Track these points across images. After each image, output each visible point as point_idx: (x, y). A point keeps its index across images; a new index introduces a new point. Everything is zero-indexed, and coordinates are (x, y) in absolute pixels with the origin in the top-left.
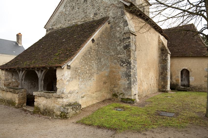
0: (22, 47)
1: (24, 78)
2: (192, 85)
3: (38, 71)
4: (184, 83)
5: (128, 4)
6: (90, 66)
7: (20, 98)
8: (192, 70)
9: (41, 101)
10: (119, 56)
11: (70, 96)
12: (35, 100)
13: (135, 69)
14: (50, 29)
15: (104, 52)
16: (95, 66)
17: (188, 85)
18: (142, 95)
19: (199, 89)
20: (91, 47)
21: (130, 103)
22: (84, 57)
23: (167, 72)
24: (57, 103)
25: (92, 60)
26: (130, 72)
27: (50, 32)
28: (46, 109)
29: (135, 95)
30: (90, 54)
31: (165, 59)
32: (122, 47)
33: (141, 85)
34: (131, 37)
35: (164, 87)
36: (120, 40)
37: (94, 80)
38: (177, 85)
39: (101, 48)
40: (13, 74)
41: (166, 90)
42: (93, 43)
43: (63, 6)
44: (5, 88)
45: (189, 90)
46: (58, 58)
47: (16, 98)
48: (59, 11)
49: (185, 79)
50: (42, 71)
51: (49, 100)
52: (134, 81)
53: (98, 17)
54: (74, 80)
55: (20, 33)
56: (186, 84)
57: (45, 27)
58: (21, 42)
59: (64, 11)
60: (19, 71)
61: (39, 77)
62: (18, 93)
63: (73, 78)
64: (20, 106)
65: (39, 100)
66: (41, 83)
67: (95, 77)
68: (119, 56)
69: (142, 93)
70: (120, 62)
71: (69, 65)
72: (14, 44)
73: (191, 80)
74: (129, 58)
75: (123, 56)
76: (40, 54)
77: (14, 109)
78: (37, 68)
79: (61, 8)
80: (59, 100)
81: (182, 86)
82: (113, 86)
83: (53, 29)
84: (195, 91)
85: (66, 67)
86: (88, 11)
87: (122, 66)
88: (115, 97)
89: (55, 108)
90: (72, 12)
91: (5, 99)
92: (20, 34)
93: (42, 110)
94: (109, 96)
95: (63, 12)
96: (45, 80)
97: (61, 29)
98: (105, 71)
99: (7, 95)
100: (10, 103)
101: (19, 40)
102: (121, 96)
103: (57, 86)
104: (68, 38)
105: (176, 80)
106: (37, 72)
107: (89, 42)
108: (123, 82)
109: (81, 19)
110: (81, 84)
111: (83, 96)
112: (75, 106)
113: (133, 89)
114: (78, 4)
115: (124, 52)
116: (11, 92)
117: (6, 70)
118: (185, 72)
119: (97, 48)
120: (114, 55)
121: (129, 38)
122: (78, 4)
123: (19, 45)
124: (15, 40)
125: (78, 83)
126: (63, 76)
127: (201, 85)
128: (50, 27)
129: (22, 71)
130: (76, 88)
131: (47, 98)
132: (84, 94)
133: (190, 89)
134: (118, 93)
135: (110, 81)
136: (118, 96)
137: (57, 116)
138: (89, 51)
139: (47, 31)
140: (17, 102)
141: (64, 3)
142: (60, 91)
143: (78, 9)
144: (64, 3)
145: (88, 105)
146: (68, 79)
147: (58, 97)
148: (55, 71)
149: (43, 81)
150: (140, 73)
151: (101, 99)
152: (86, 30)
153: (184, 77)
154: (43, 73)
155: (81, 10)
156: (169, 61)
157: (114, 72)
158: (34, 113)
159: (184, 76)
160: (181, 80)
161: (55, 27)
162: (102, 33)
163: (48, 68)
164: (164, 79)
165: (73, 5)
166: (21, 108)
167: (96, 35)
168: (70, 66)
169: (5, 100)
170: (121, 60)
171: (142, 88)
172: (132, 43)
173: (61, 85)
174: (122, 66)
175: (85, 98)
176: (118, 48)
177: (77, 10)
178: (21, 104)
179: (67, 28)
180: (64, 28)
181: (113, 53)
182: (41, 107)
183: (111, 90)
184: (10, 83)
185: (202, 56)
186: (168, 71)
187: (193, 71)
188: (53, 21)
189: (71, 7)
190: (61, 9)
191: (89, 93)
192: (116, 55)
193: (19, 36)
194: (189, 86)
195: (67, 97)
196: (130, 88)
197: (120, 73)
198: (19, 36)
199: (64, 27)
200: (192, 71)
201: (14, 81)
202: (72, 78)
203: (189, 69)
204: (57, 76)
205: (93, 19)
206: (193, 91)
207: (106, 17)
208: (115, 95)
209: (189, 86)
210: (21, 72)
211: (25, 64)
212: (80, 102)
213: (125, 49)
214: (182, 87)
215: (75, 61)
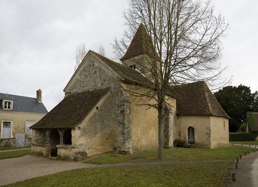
0: (42, 104)
1: (49, 135)
2: (196, 142)
3: (59, 130)
4: (191, 140)
5: (124, 80)
6: (95, 127)
7: (47, 150)
8: (196, 128)
9: (62, 151)
10: (117, 119)
11: (80, 147)
12: (58, 151)
13: (129, 129)
14: (68, 93)
15: (106, 116)
16: (99, 127)
17: (194, 143)
18: (140, 149)
19: (202, 146)
20: (95, 113)
21: (124, 154)
22: (91, 120)
23: (169, 130)
24: (72, 151)
25: (96, 123)
26: (124, 130)
27: (69, 95)
28: (65, 156)
29: (129, 148)
30: (95, 118)
31: (167, 118)
32: (119, 111)
33: (139, 140)
34: (125, 104)
35: (167, 143)
36: (118, 107)
37: (98, 136)
38: (185, 142)
39: (104, 112)
40: (41, 132)
41: (168, 146)
42: (97, 109)
43: (79, 74)
44: (35, 143)
45: (193, 147)
46: (73, 121)
47: (44, 150)
48: (75, 78)
49: (192, 136)
50: (62, 130)
51: (67, 150)
52: (128, 138)
53: (104, 87)
54: (83, 136)
55: (40, 90)
56: (192, 141)
57: (64, 91)
58: (41, 99)
59: (79, 78)
60: (46, 130)
61: (60, 134)
62: (45, 147)
63: (82, 135)
64: (47, 156)
65: (60, 151)
66: (62, 139)
67: (99, 135)
68: (117, 119)
69: (140, 148)
70: (118, 123)
71: (79, 127)
72: (35, 101)
73: (195, 137)
74: (124, 121)
75: (120, 118)
76: (60, 117)
77: (43, 159)
78: (59, 128)
79: (77, 75)
80: (73, 149)
81: (189, 143)
82: (114, 142)
83: (70, 92)
84: (199, 148)
85: (77, 128)
86: (97, 81)
87: (119, 126)
88: (115, 150)
89: (71, 155)
90: (85, 80)
91: (36, 151)
92: (40, 91)
93: (62, 157)
94: (111, 149)
95: (79, 79)
96: (64, 137)
97: (76, 94)
98: (107, 130)
99: (37, 148)
100: (40, 154)
101: (39, 97)
102: (119, 149)
103: (72, 141)
104: (81, 104)
105: (184, 138)
106: (59, 131)
107: (94, 110)
108: (120, 138)
109: (92, 86)
110: (88, 139)
111: (89, 148)
112: (84, 154)
113: (126, 144)
114: (90, 74)
115: (121, 116)
116: (40, 146)
117: (37, 129)
118: (191, 130)
119: (101, 113)
120: (115, 118)
121: (124, 105)
122: (90, 74)
123: (39, 102)
124: (35, 96)
125: (86, 138)
126: (76, 134)
127: (203, 142)
128: (69, 91)
129: (49, 130)
130: (84, 142)
131: (65, 149)
132: (90, 147)
133: (195, 146)
134: (117, 147)
135: (110, 138)
136: (116, 149)
137: (72, 160)
138: (94, 116)
139: (66, 94)
140: (45, 153)
141: (80, 72)
142: (74, 144)
143: (90, 78)
144: (80, 72)
145: (93, 155)
146: (79, 136)
147: (72, 148)
148: (71, 130)
149: (63, 137)
150: (138, 132)
151: (103, 151)
152: (96, 95)
153: (190, 134)
154: (63, 132)
155: (92, 79)
156: (171, 120)
157: (114, 131)
158: (57, 160)
159: (190, 133)
160: (189, 138)
161: (72, 91)
162: (105, 101)
163: (66, 129)
164: (166, 136)
165: (86, 74)
166: (48, 158)
167: (100, 104)
168: (80, 127)
169: (35, 152)
170: (119, 122)
171: (140, 144)
172: (127, 108)
173: (74, 140)
174: (119, 126)
175: (91, 149)
176: (117, 112)
177: (89, 79)
178: (47, 154)
179: (82, 93)
180: (80, 93)
181: (114, 116)
182: (62, 155)
183: (113, 145)
184: (39, 139)
185: (203, 115)
186: (169, 129)
187: (197, 129)
188: (70, 85)
189: (85, 75)
190: (77, 76)
191: (94, 146)
192: (116, 118)
193: (39, 93)
194: (194, 144)
195: (78, 148)
196: (124, 143)
197: (118, 132)
198: (39, 93)
199: (79, 92)
200: (196, 129)
201: (41, 138)
202: (81, 136)
203: (194, 127)
204: (72, 134)
205: (100, 87)
206: (196, 148)
207: (109, 88)
208: (115, 149)
209: (194, 144)
210: (47, 131)
211: (51, 125)
212: (87, 152)
213: (121, 113)
214: (189, 144)
215: (83, 125)
